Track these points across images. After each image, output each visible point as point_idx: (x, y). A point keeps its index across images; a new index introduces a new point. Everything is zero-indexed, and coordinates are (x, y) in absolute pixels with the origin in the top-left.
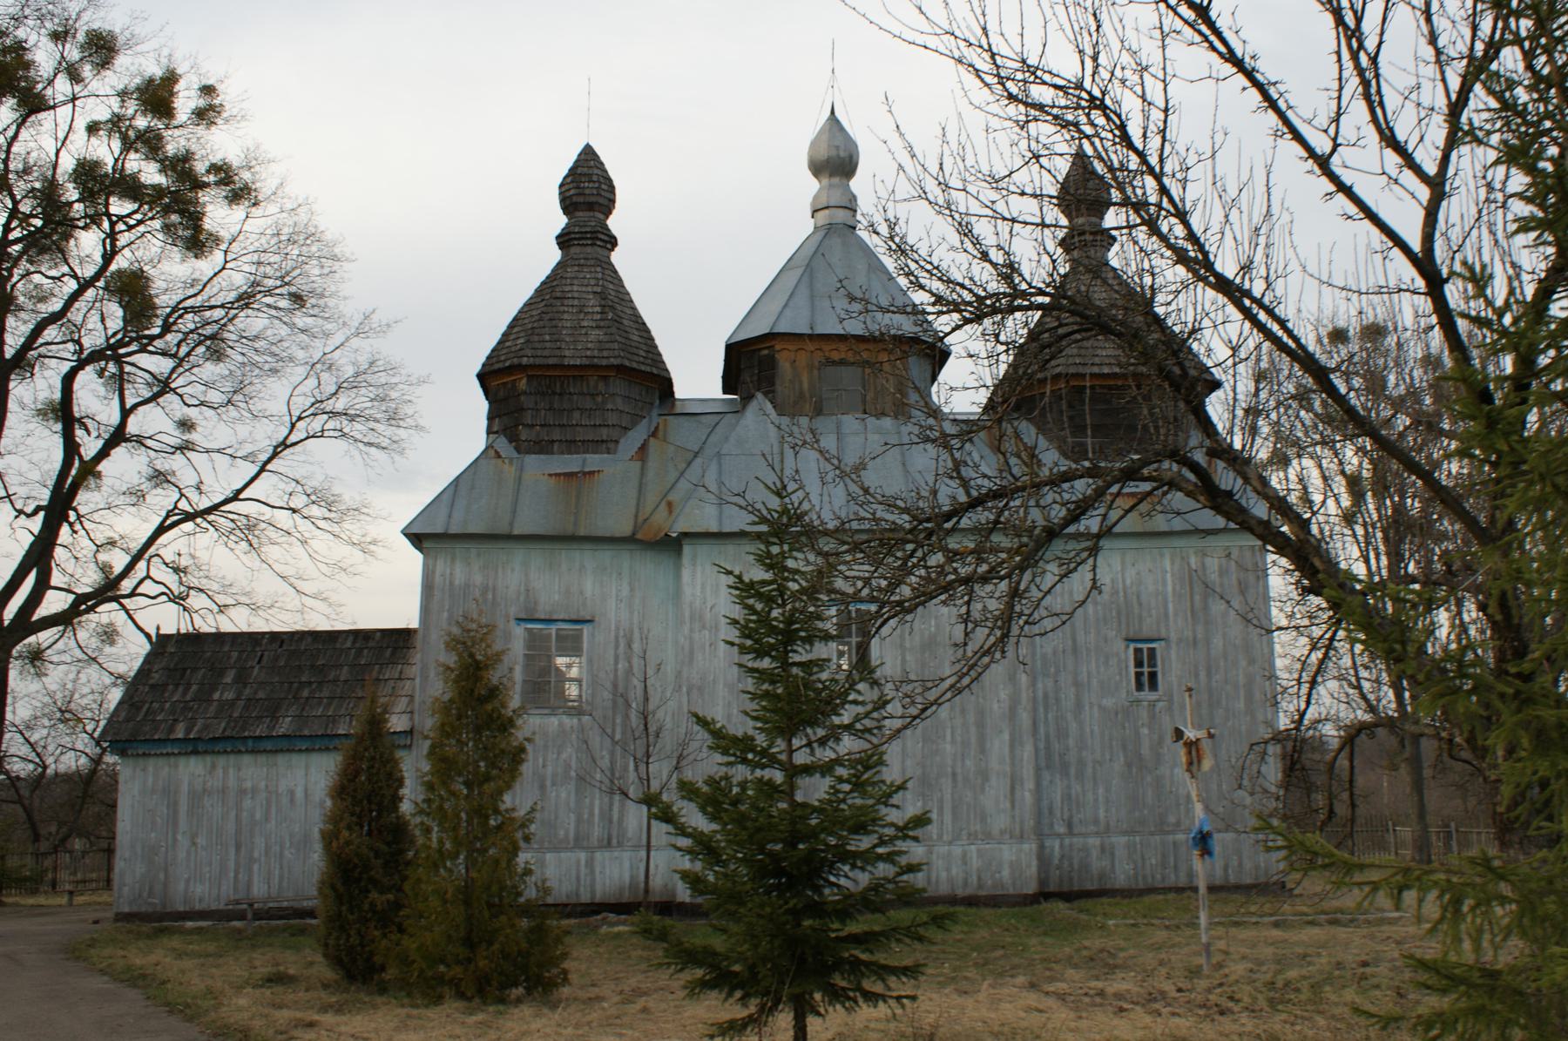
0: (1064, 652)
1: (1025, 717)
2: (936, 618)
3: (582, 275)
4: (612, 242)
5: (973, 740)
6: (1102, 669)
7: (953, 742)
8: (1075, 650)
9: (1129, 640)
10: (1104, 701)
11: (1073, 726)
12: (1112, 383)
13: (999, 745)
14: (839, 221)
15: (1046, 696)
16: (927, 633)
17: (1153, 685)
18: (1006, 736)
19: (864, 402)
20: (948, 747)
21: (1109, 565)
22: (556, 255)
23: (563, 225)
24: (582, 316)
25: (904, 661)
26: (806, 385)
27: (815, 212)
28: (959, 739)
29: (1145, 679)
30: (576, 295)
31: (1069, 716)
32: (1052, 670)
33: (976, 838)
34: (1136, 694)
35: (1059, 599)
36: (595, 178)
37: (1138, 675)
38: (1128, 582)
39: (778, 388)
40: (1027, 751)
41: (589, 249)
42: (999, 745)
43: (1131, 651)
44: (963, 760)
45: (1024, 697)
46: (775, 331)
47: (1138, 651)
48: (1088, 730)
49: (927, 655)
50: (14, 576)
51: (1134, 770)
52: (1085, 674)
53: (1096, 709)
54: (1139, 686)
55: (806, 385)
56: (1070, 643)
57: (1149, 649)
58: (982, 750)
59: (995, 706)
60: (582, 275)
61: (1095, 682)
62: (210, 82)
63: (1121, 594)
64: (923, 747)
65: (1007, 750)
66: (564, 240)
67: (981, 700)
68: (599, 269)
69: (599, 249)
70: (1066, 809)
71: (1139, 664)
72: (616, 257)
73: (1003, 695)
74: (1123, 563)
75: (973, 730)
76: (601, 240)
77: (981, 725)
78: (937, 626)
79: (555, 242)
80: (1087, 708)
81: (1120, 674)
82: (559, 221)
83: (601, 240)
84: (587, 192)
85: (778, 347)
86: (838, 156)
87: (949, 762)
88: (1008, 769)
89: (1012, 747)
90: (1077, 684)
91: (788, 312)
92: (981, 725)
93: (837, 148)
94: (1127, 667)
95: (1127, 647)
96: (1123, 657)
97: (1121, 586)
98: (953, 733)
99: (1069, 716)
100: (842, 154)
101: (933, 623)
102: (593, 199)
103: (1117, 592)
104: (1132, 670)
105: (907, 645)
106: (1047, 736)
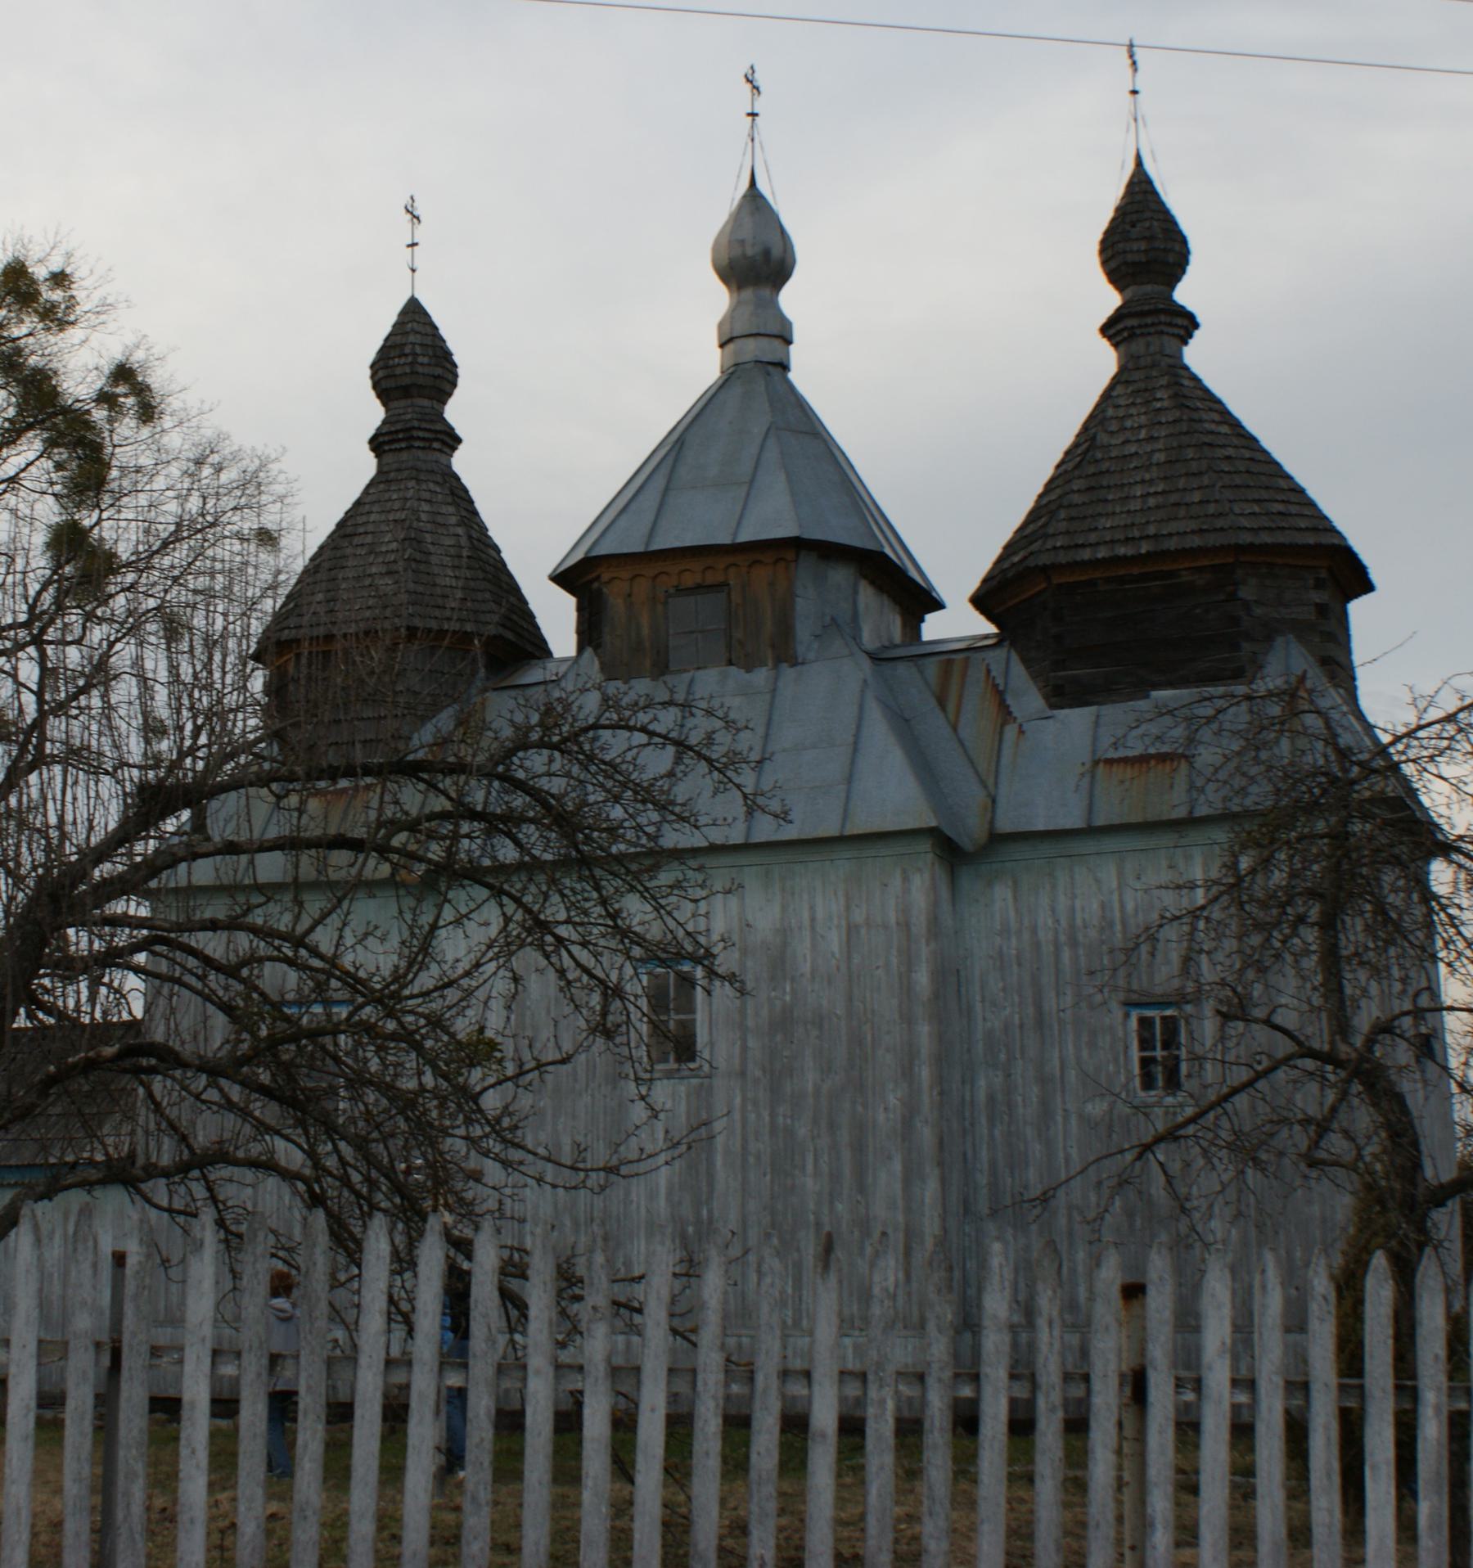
0: (1021, 1026)
1: (926, 1135)
2: (793, 980)
3: (387, 496)
4: (452, 440)
5: (847, 1171)
6: (1085, 1053)
7: (817, 1174)
8: (1040, 1022)
9: (1129, 1004)
10: (1089, 1107)
11: (1037, 1149)
12: (1122, 572)
13: (887, 1179)
14: (747, 358)
15: (991, 1099)
16: (778, 1003)
17: (1173, 1082)
18: (897, 1166)
19: (729, 648)
20: (809, 1182)
21: (1097, 881)
22: (367, 466)
23: (377, 422)
24: (371, 559)
25: (744, 1048)
26: (646, 631)
27: (722, 346)
28: (825, 1169)
29: (1159, 1073)
30: (370, 528)
31: (1030, 1132)
32: (1003, 1057)
33: (853, 1327)
34: (1142, 1094)
35: (1014, 941)
36: (407, 350)
37: (1146, 1063)
38: (1130, 906)
39: (607, 638)
40: (930, 1190)
41: (404, 456)
42: (887, 1179)
43: (1133, 1023)
44: (831, 1203)
45: (926, 1101)
46: (655, 547)
47: (1145, 1023)
48: (1061, 1155)
49: (779, 1038)
50: (1397, 1337)
51: (1138, 1222)
52: (1057, 1063)
53: (1074, 1121)
54: (1148, 1082)
55: (646, 631)
56: (1031, 1010)
57: (1163, 1018)
58: (861, 1187)
59: (881, 1117)
60: (387, 496)
61: (1072, 1075)
62: (56, 268)
63: (1118, 927)
64: (772, 1181)
65: (898, 1187)
66: (377, 443)
67: (860, 1109)
68: (412, 484)
69: (420, 453)
70: (1022, 1285)
71: (1145, 1043)
72: (462, 463)
73: (892, 1100)
74: (1121, 874)
75: (846, 1155)
76: (419, 438)
77: (859, 1148)
78: (794, 992)
79: (367, 447)
80: (1059, 1119)
81: (1116, 1060)
82: (373, 414)
83: (419, 438)
84: (398, 371)
85: (605, 577)
86: (744, 256)
87: (812, 1206)
88: (901, 1218)
89: (907, 1182)
90: (1043, 1080)
91: (623, 522)
92: (859, 1148)
93: (742, 242)
94: (1126, 1048)
95: (1127, 1016)
96: (1120, 1034)
97: (1117, 914)
98: (816, 1161)
99: (1030, 1132)
100: (750, 252)
101: (788, 989)
102: (407, 381)
103: (1111, 925)
104: (1135, 1054)
105: (750, 1023)
106: (993, 1164)
